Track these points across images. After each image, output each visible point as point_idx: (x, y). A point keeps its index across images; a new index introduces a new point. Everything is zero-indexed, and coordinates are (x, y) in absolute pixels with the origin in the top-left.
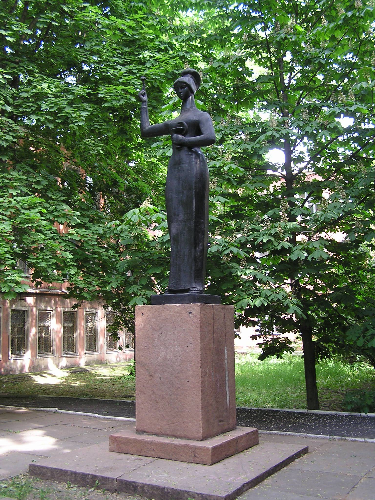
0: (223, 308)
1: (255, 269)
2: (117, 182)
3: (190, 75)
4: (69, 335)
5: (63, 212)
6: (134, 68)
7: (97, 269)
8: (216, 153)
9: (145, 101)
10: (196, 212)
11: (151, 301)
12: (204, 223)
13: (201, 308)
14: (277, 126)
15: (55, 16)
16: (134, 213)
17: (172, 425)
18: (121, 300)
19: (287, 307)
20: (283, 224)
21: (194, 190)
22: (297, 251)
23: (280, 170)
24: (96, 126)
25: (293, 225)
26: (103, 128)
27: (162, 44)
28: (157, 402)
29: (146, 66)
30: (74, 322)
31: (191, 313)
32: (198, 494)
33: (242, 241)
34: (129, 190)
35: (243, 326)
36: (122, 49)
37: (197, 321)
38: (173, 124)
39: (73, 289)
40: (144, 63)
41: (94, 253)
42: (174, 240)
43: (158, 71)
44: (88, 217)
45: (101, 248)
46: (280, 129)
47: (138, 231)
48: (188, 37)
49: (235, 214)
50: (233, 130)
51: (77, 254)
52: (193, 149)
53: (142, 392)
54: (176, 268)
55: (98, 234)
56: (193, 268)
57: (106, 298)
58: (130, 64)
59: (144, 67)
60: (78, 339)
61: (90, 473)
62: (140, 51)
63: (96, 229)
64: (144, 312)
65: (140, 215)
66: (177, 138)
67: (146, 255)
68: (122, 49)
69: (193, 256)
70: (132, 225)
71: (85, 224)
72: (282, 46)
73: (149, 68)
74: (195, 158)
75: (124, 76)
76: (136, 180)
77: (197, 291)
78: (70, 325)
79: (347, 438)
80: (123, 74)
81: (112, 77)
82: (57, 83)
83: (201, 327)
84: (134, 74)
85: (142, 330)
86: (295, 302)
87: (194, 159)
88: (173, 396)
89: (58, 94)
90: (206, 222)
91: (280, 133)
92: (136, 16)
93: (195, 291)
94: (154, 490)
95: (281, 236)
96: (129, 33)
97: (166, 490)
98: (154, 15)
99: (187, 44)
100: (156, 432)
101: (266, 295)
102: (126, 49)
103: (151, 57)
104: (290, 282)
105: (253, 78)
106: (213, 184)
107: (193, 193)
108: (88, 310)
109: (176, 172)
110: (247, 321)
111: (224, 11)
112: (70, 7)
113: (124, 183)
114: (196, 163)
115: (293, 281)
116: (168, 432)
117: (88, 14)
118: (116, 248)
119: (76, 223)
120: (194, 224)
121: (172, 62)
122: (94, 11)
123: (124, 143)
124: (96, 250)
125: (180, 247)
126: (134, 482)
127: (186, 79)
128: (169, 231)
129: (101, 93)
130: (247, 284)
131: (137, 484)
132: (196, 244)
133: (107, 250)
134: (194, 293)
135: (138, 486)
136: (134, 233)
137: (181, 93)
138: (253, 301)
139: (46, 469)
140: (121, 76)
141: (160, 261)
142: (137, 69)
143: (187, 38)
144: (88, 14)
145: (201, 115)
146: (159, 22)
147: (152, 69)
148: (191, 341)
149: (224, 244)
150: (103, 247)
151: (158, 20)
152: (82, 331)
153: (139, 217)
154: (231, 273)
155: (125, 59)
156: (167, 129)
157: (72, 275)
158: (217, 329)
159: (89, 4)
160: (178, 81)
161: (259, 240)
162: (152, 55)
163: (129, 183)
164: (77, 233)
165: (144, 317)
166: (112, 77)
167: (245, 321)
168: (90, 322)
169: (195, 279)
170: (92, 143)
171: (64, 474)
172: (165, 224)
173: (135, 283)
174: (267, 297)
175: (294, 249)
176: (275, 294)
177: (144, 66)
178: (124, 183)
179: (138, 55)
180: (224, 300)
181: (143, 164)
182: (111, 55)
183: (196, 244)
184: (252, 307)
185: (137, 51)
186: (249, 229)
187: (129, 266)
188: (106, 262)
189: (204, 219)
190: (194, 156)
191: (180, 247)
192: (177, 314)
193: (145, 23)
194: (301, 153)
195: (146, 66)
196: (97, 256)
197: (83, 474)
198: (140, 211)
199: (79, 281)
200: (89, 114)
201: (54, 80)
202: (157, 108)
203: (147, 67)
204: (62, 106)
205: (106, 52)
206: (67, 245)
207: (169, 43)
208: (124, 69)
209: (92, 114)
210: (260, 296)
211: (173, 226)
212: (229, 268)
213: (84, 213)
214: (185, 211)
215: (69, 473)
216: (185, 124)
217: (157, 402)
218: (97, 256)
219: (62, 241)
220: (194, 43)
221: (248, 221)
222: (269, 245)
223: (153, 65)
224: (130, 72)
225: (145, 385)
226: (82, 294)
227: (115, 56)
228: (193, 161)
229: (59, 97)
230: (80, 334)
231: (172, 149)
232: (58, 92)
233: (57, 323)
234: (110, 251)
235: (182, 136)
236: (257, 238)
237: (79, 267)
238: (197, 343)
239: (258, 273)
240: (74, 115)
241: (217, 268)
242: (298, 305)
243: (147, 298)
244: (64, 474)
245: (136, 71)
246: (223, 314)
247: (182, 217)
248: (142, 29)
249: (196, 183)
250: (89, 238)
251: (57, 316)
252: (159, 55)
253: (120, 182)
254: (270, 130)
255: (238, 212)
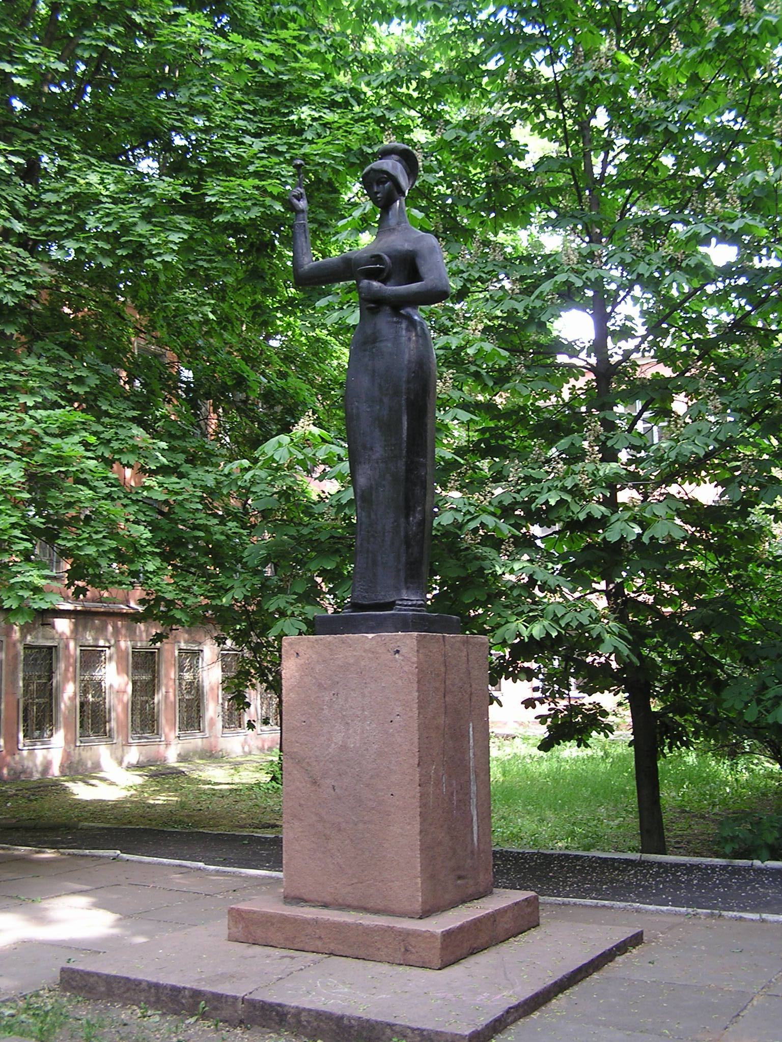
0: (466, 642)
1: (531, 561)
2: (244, 379)
3: (395, 157)
4: (144, 698)
5: (131, 442)
6: (279, 142)
7: (203, 560)
8: (450, 319)
9: (303, 211)
10: (408, 442)
11: (315, 627)
12: (425, 465)
13: (418, 642)
14: (578, 263)
15: (115, 34)
16: (280, 445)
17: (360, 885)
18: (252, 626)
19: (599, 640)
20: (590, 468)
21: (405, 397)
22: (619, 522)
23: (583, 355)
24: (201, 263)
25: (612, 468)
26: (216, 268)
27: (338, 92)
28: (327, 838)
29: (304, 137)
30: (153, 671)
31: (398, 652)
32: (413, 1030)
33: (506, 503)
34: (268, 396)
35: (506, 679)
36: (253, 102)
37: (411, 669)
38: (361, 258)
39: (152, 602)
40: (300, 132)
41: (196, 527)
42: (364, 499)
43: (329, 148)
44: (183, 452)
45: (210, 518)
46: (584, 269)
47: (289, 481)
48: (393, 77)
49: (490, 445)
50: (486, 270)
51: (161, 529)
52: (402, 312)
53: (295, 816)
54: (367, 558)
55: (204, 488)
56: (403, 559)
57: (221, 620)
58: (271, 134)
59: (301, 141)
60: (162, 706)
61: (188, 986)
62: (291, 106)
63: (200, 477)
64: (301, 650)
65: (291, 449)
66: (369, 287)
67: (305, 531)
68: (253, 102)
69: (402, 534)
70: (275, 468)
71: (178, 466)
72: (588, 96)
73: (311, 142)
74: (408, 330)
75: (258, 158)
76: (283, 375)
77: (410, 606)
78: (145, 677)
79: (724, 913)
80: (256, 154)
81: (233, 159)
82: (119, 172)
83: (418, 682)
84: (279, 154)
85: (297, 689)
86: (616, 630)
87: (404, 332)
88: (361, 826)
89: (122, 196)
90: (429, 462)
91: (584, 277)
92: (284, 34)
93: (406, 606)
94: (321, 1020)
95: (587, 493)
96: (269, 68)
97: (346, 1022)
98: (321, 30)
99: (391, 93)
100: (325, 900)
101: (555, 615)
102: (264, 103)
103: (314, 119)
104: (605, 588)
105: (527, 163)
106: (444, 384)
107: (403, 402)
108: (183, 645)
109: (366, 359)
110: (515, 668)
111: (466, 23)
112: (147, 14)
113: (258, 381)
114: (410, 339)
115: (611, 586)
116: (350, 900)
117: (183, 30)
118: (241, 517)
119: (158, 465)
120: (404, 468)
121: (358, 129)
122: (197, 24)
123: (259, 297)
124: (201, 522)
125: (376, 515)
126: (279, 1005)
127: (387, 164)
128: (353, 482)
129: (210, 193)
130: (515, 593)
131: (285, 1009)
132: (408, 509)
133: (223, 522)
134: (405, 610)
135: (288, 1013)
136: (280, 485)
137: (377, 193)
138: (527, 627)
139: (96, 978)
140: (252, 157)
141: (334, 543)
142: (285, 143)
143: (389, 80)
144: (183, 30)
145: (420, 239)
146: (331, 45)
147: (316, 143)
148: (398, 710)
149: (467, 508)
150: (215, 515)
151: (329, 42)
152: (171, 690)
153: (290, 452)
154: (482, 569)
155: (261, 122)
156: (347, 269)
157: (151, 573)
158: (453, 685)
159: (185, 9)
160: (372, 169)
161: (541, 500)
162: (317, 115)
163: (269, 382)
164: (161, 485)
165: (300, 661)
166: (233, 159)
167: (511, 669)
168: (188, 671)
169: (406, 582)
170: (192, 298)
171: (134, 987)
172: (345, 467)
173: (282, 590)
174: (556, 619)
175: (614, 518)
176: (573, 613)
177: (300, 138)
178: (258, 381)
179: (288, 114)
180: (467, 624)
181: (298, 341)
182: (231, 114)
183: (408, 509)
184: (526, 640)
185: (286, 107)
186: (520, 478)
187: (269, 554)
188: (221, 547)
189: (425, 457)
190: (404, 325)
191: (376, 515)
192: (370, 655)
193: (303, 47)
194: (629, 318)
195: (304, 137)
196: (202, 534)
197: (174, 988)
198: (292, 440)
199: (165, 586)
200: (186, 237)
201: (112, 166)
202: (327, 226)
203: (306, 140)
204: (130, 220)
205: (221, 109)
206: (139, 510)
207: (352, 90)
208: (259, 145)
209: (191, 237)
210: (542, 617)
211: (360, 471)
212: (477, 558)
213: (176, 443)
214: (385, 441)
215: (144, 985)
216: (387, 258)
217: (327, 838)
218: (202, 534)
219: (128, 502)
220: (404, 90)
221: (517, 461)
222: (561, 510)
223: (319, 136)
224: (271, 150)
225: (303, 802)
226: (171, 613)
227: (240, 116)
228: (402, 336)
229: (123, 201)
230: (166, 697)
231: (358, 312)
232: (122, 191)
233: (118, 673)
234: (230, 524)
235: (380, 284)
236: (537, 495)
237: (166, 557)
238: (410, 714)
239: (537, 569)
240: (154, 241)
241: (452, 558)
242: (621, 636)
243: (306, 621)
244: (134, 987)
245: (283, 149)
246: (465, 653)
247: (379, 452)
248: (296, 60)
249: (408, 382)
250: (185, 496)
251: (118, 658)
252: (331, 114)
253: (251, 379)
254: (563, 271)
255: (497, 442)
